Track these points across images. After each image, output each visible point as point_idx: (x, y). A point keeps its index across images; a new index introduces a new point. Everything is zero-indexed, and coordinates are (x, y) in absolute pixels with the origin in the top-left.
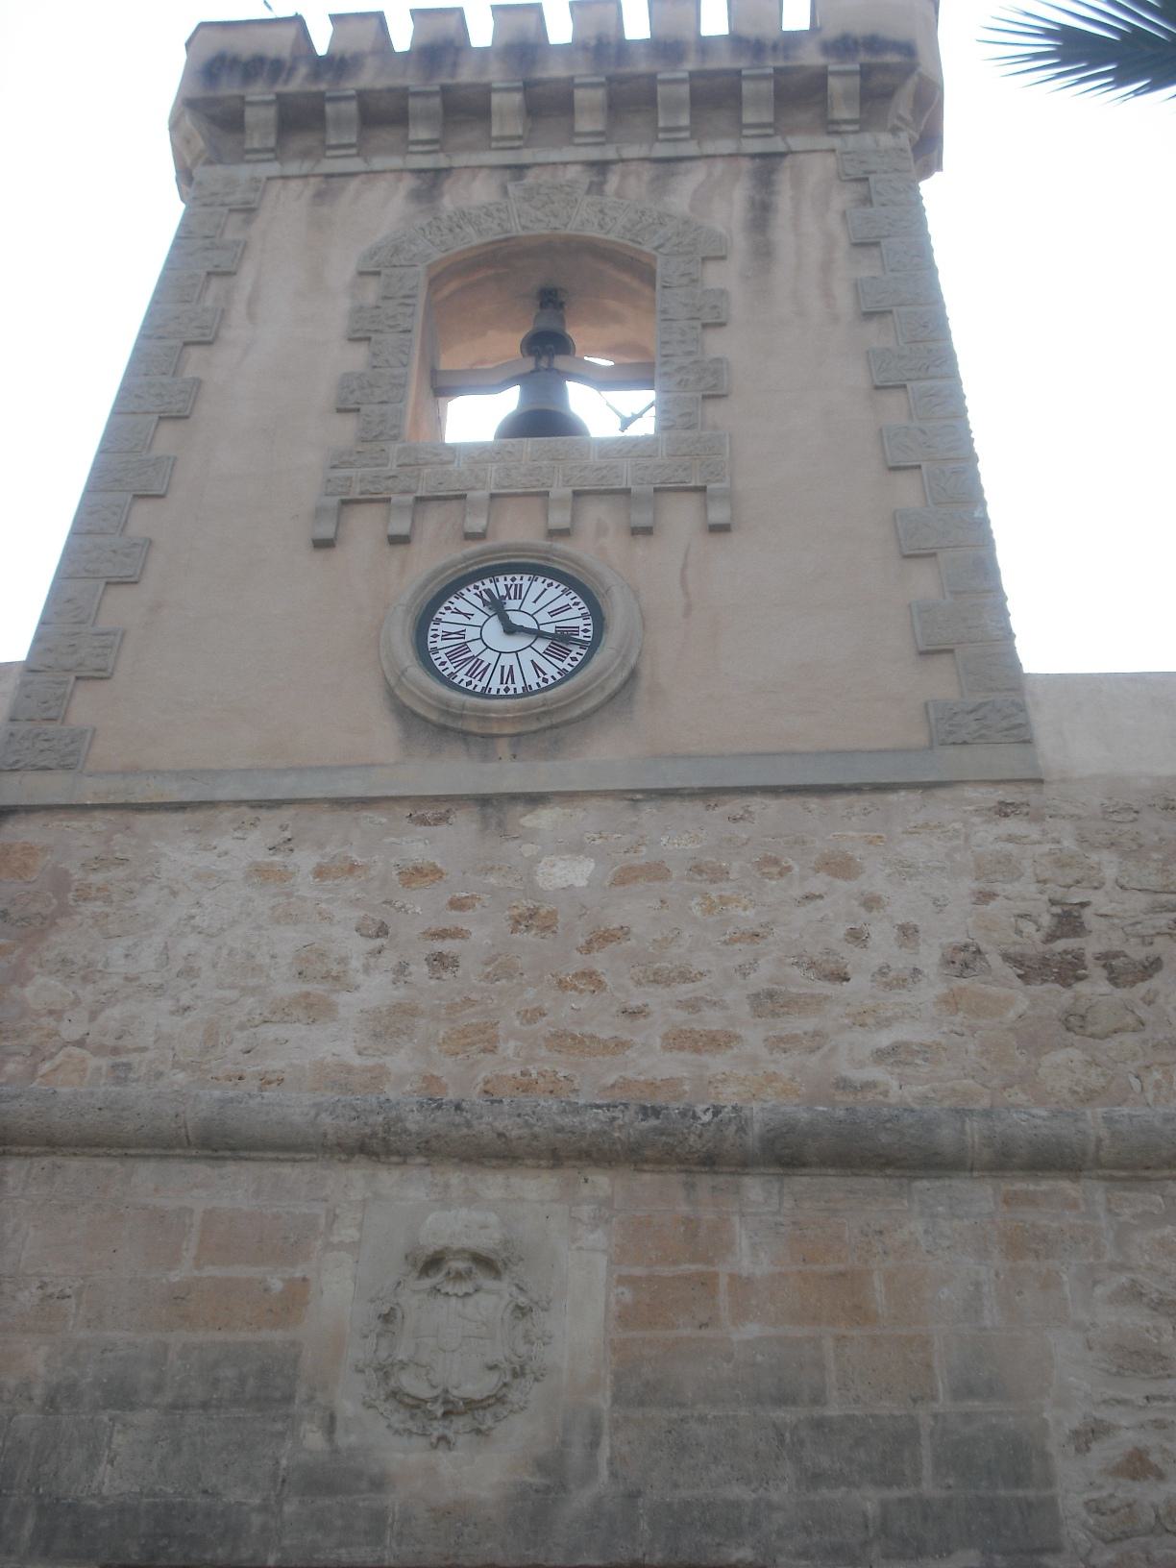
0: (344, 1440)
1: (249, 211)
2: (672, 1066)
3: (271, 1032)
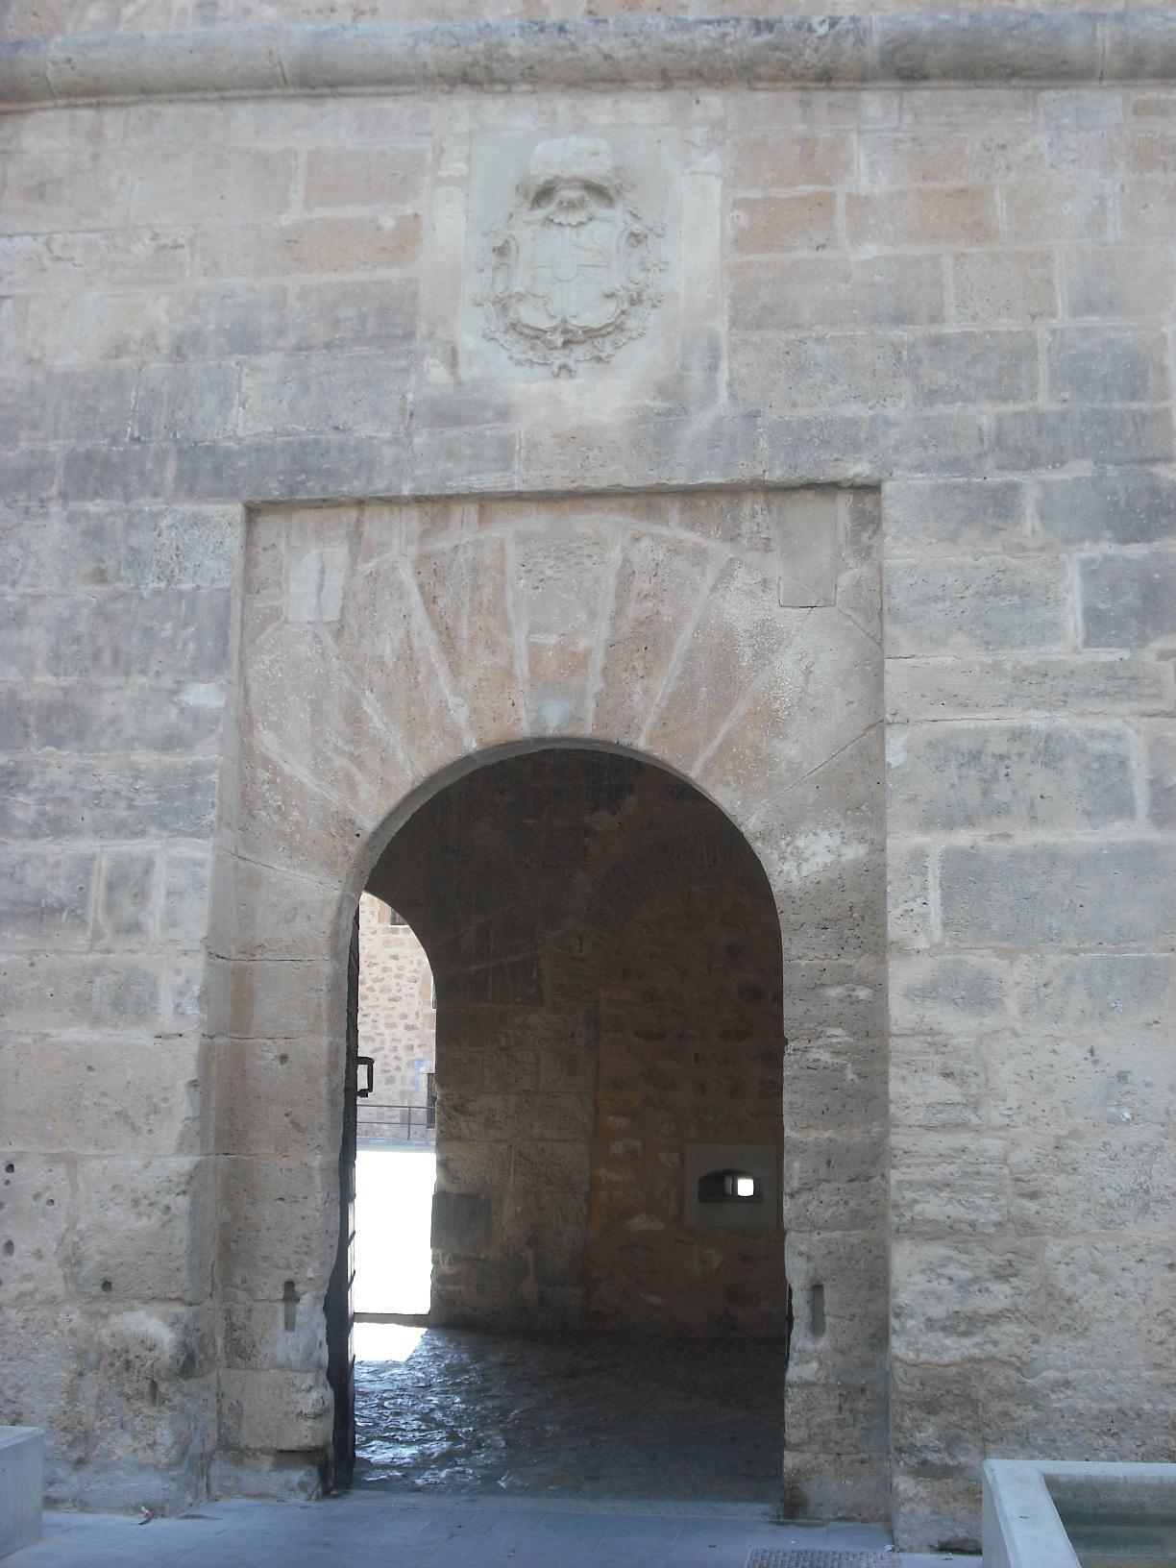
0: (467, 373)
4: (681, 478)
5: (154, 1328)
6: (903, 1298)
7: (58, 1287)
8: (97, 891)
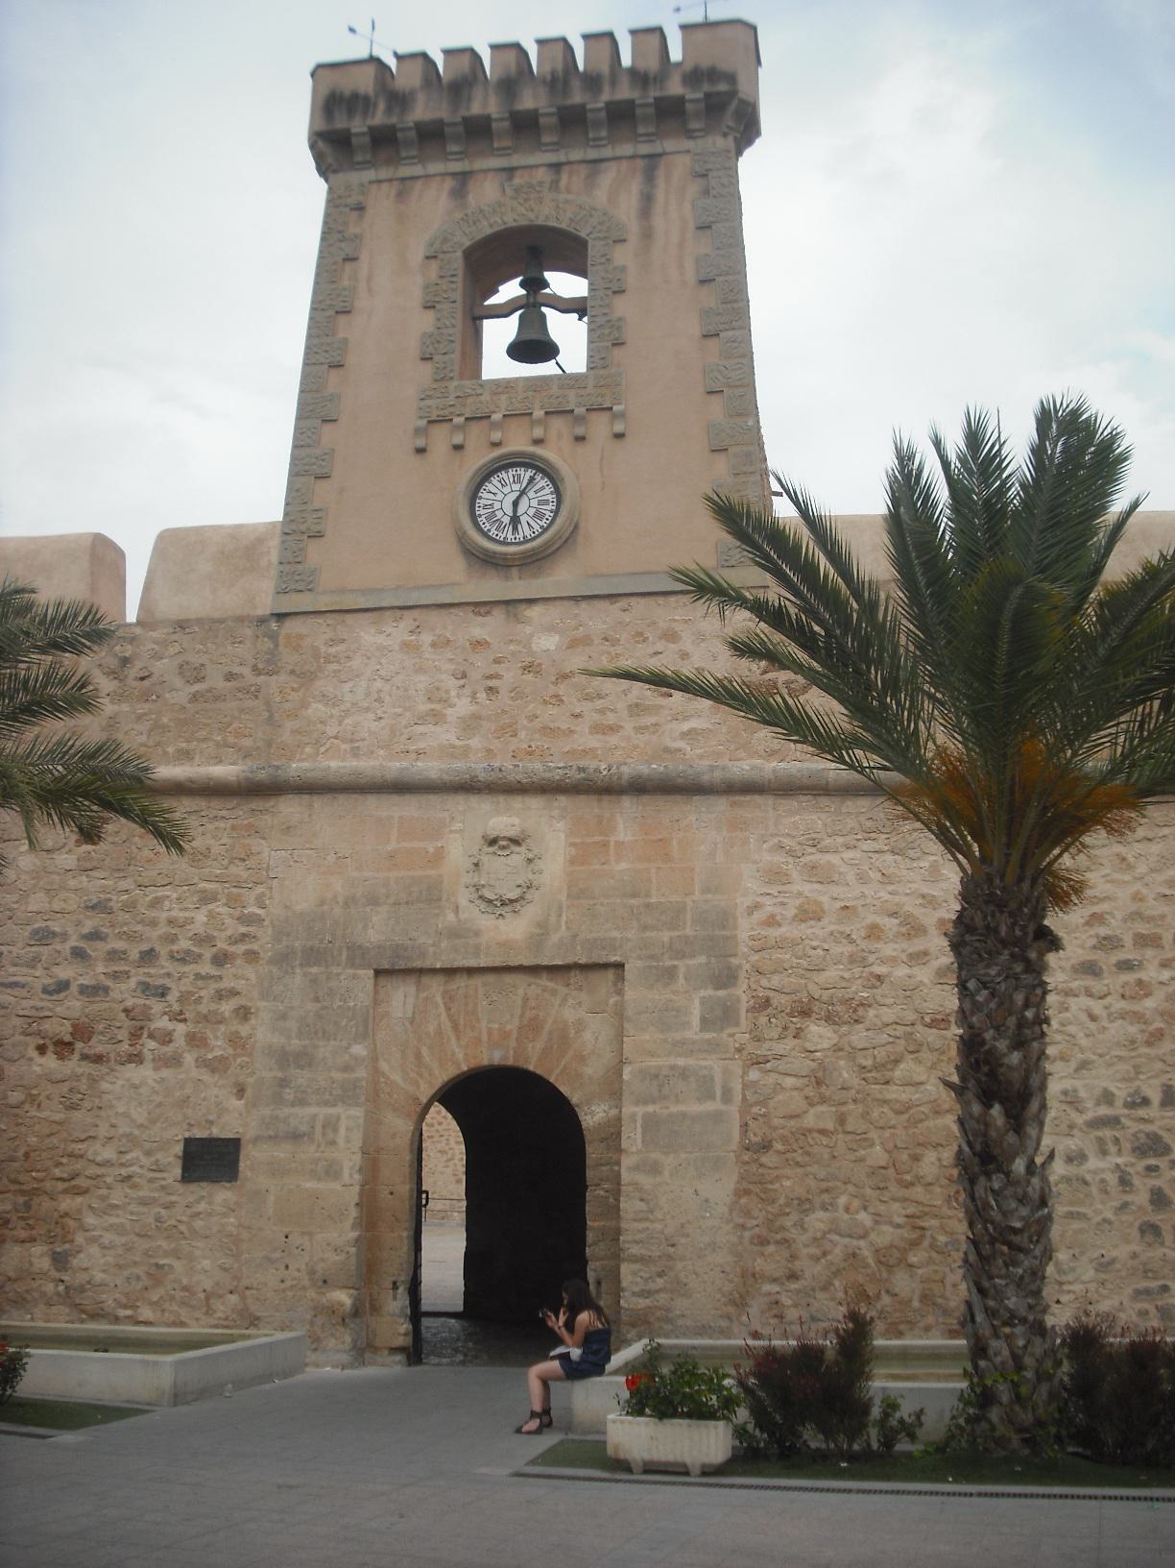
0: (463, 916)
1: (360, 208)
2: (593, 742)
3: (420, 729)
4: (546, 962)
5: (344, 1298)
6: (624, 1284)
7: (306, 1283)
8: (318, 1129)
